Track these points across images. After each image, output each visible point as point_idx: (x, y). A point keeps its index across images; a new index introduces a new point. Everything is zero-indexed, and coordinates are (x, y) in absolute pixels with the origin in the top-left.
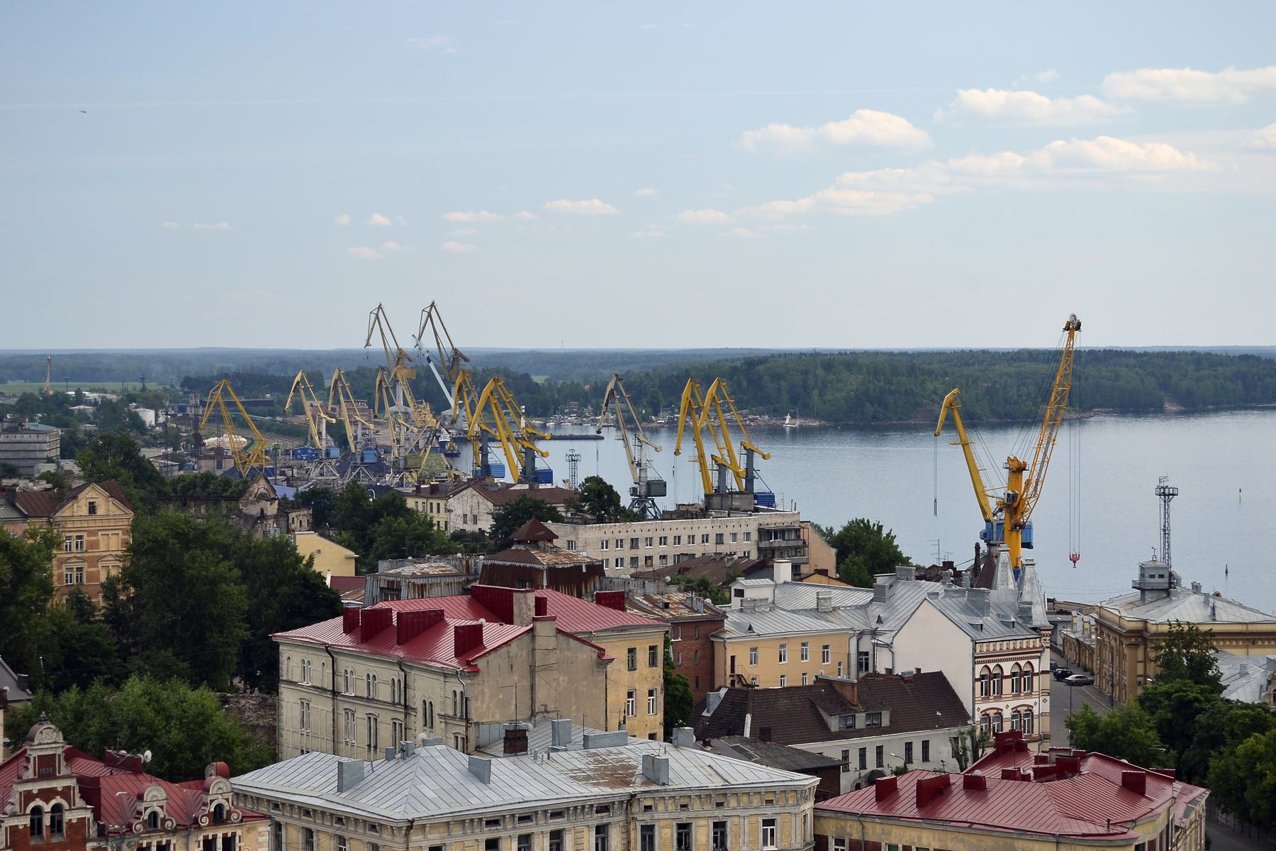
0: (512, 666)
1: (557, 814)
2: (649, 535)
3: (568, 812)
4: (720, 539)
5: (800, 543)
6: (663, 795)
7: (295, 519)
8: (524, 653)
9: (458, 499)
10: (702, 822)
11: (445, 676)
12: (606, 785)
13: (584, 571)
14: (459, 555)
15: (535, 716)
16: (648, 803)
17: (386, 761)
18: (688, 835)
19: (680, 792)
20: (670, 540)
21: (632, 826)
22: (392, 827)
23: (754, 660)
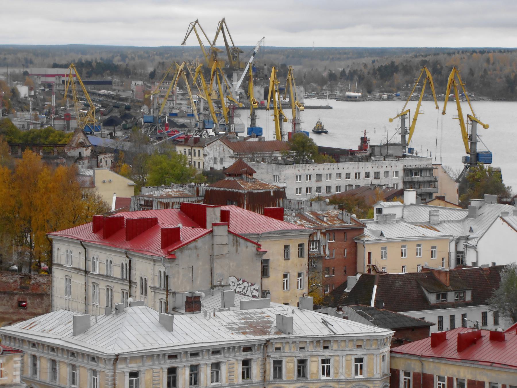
0: (198, 255)
1: (216, 352)
2: (329, 172)
3: (224, 351)
4: (348, 176)
5: (433, 179)
6: (288, 340)
7: (103, 160)
8: (206, 247)
9: (211, 148)
10: (314, 359)
11: (154, 261)
12: (250, 333)
13: (272, 194)
14: (193, 184)
15: (213, 289)
16: (278, 346)
17: (106, 316)
18: (304, 367)
19: (299, 339)
20: (343, 176)
21: (267, 361)
22: (104, 359)
23: (384, 256)
